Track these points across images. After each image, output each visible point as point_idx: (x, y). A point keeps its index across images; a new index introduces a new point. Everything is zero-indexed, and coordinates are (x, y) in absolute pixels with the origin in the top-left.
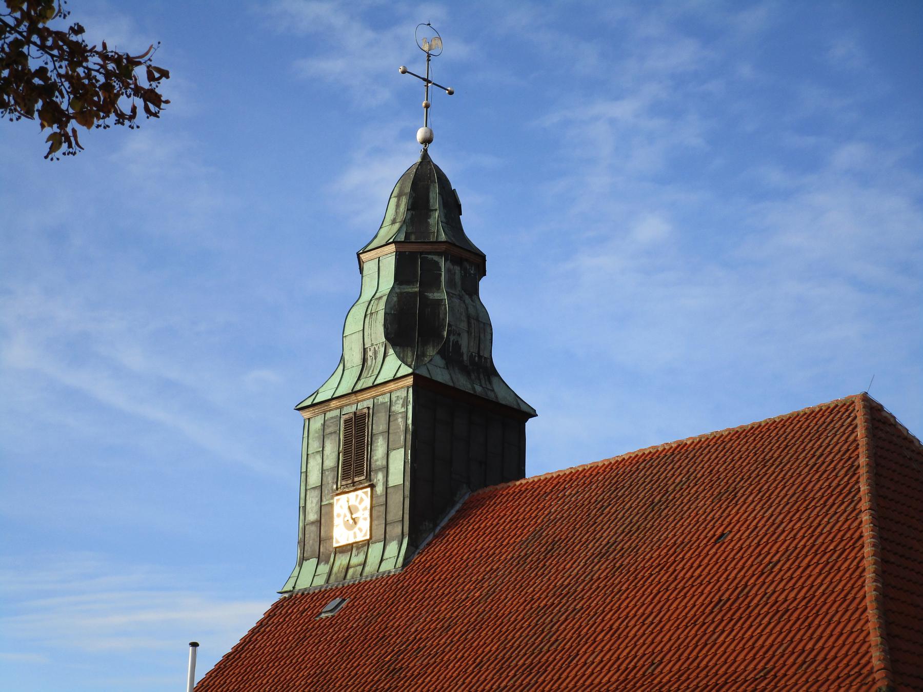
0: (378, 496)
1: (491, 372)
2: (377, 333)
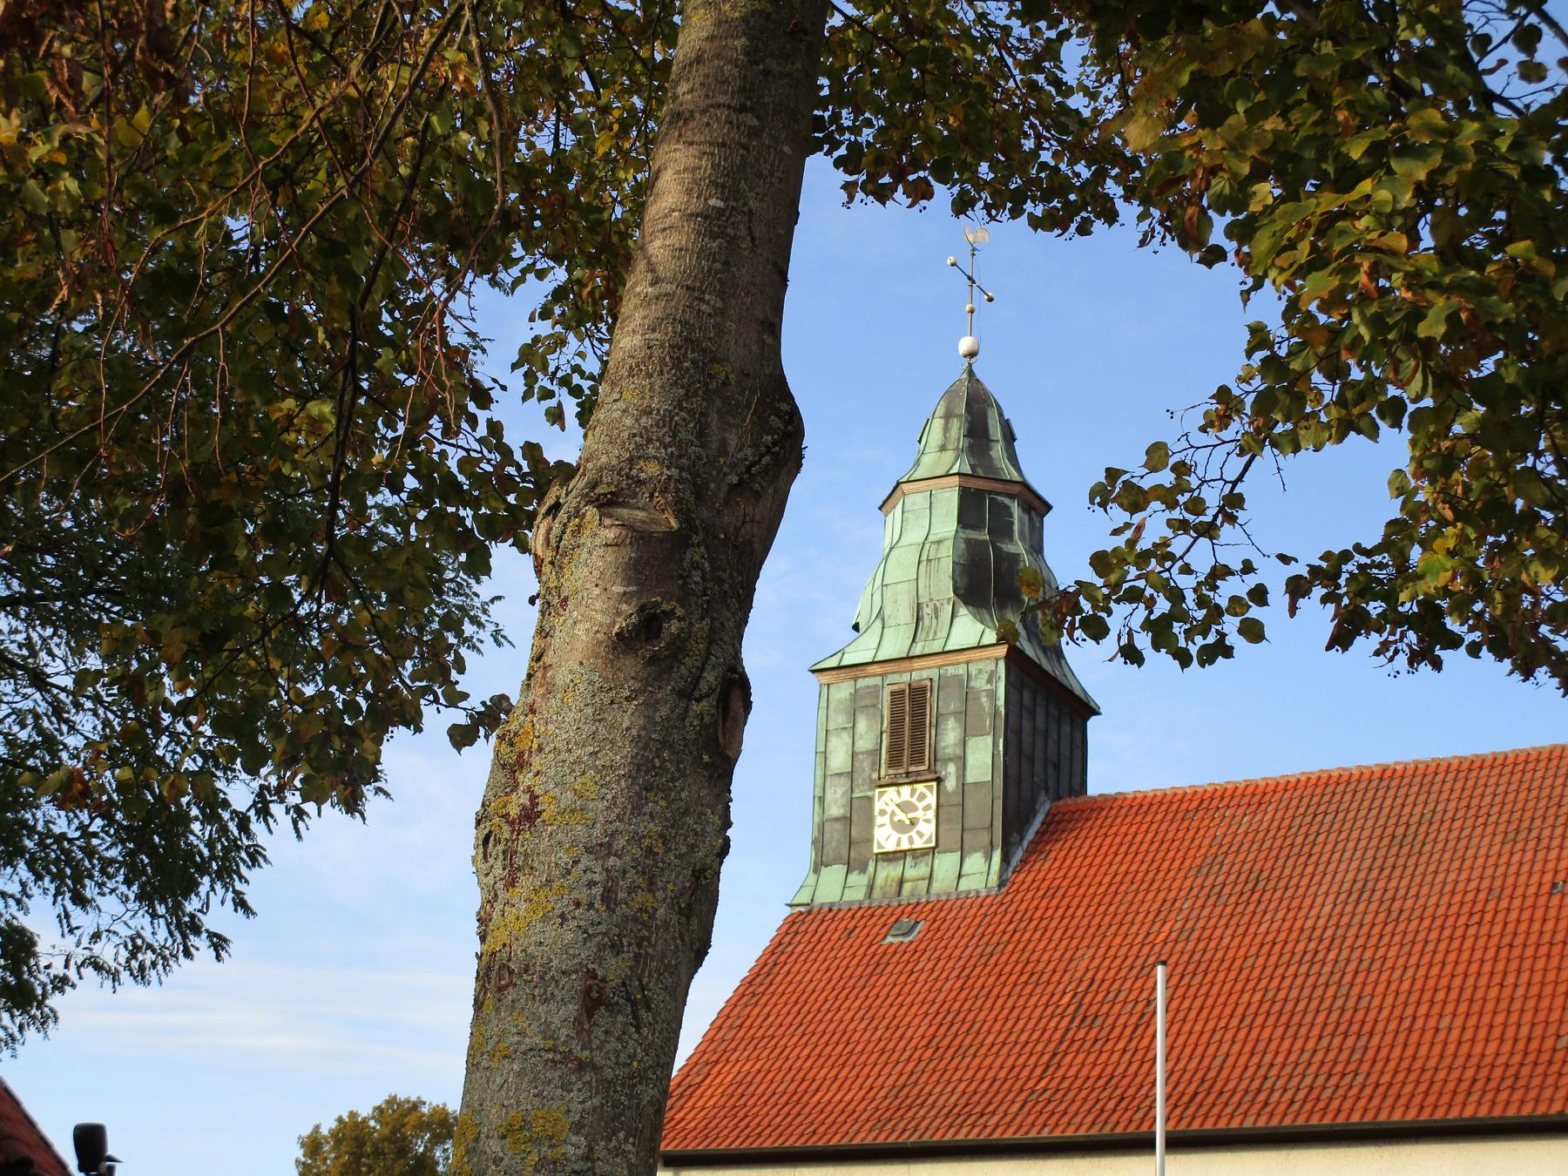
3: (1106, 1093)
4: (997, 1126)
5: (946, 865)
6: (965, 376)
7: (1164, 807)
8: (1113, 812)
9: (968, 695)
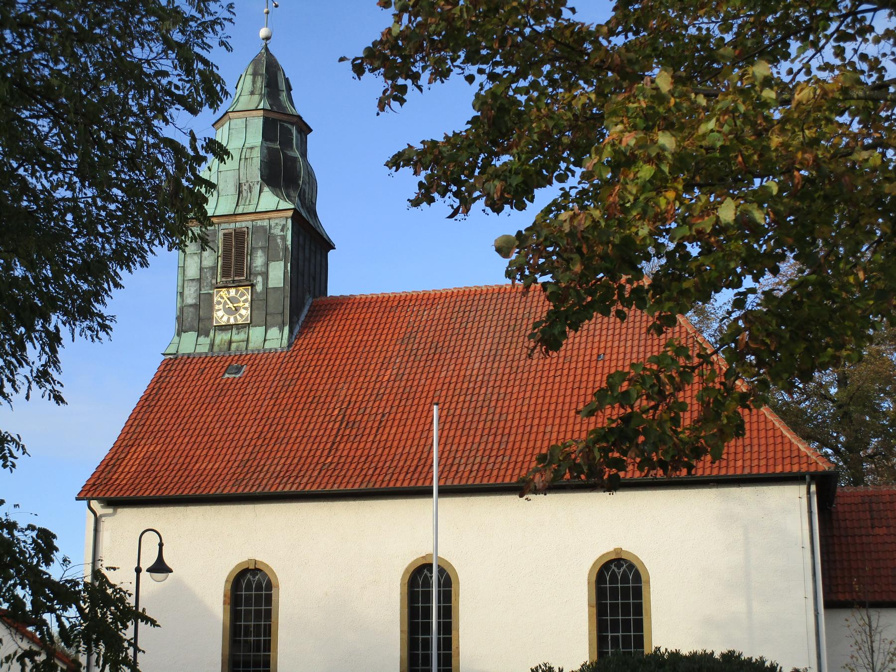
3: (367, 465)
4: (307, 484)
5: (256, 334)
6: (263, 51)
7: (378, 304)
8: (350, 306)
9: (269, 237)
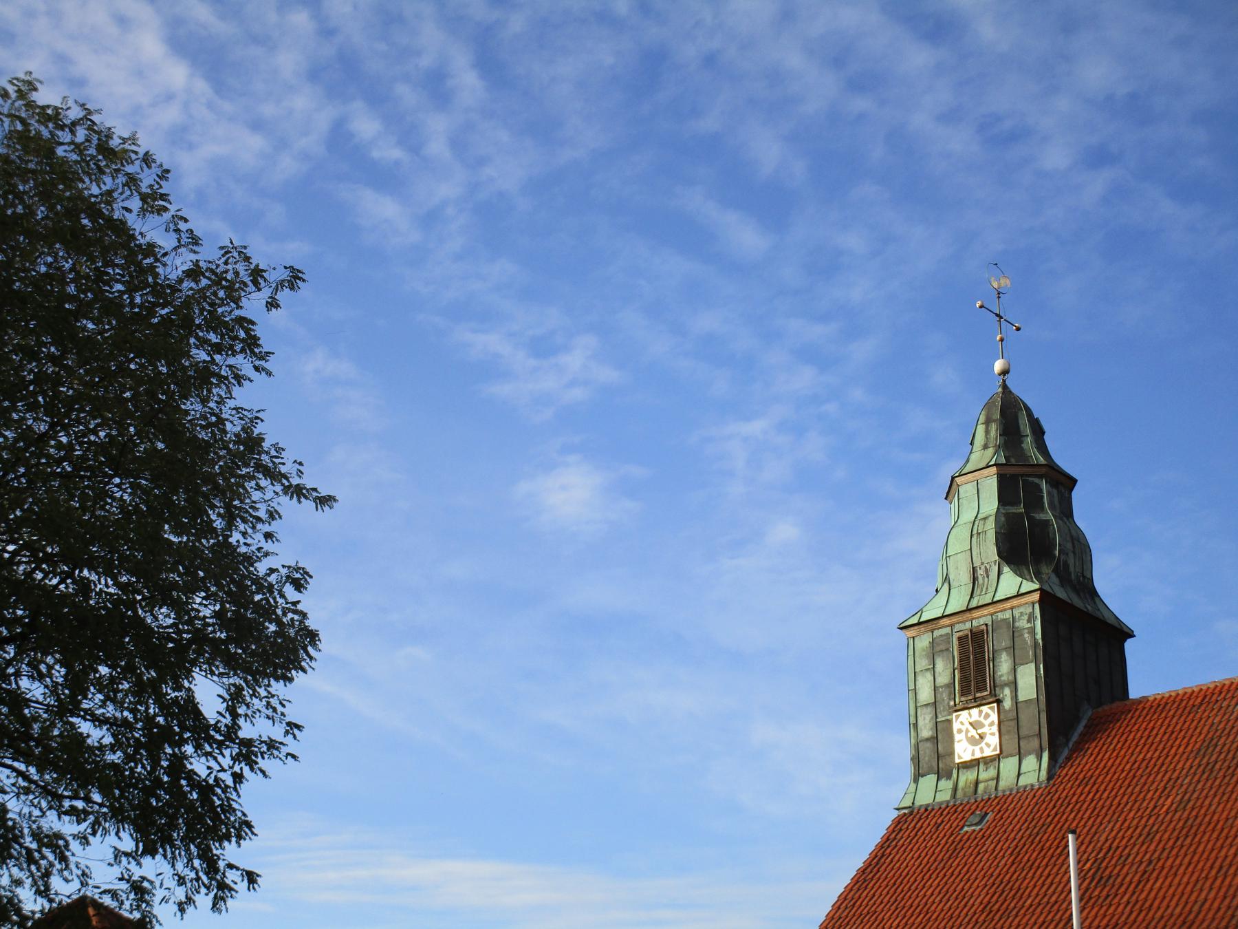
0: (1005, 711)
1: (1093, 593)
2: (989, 552)
9: (1014, 632)
